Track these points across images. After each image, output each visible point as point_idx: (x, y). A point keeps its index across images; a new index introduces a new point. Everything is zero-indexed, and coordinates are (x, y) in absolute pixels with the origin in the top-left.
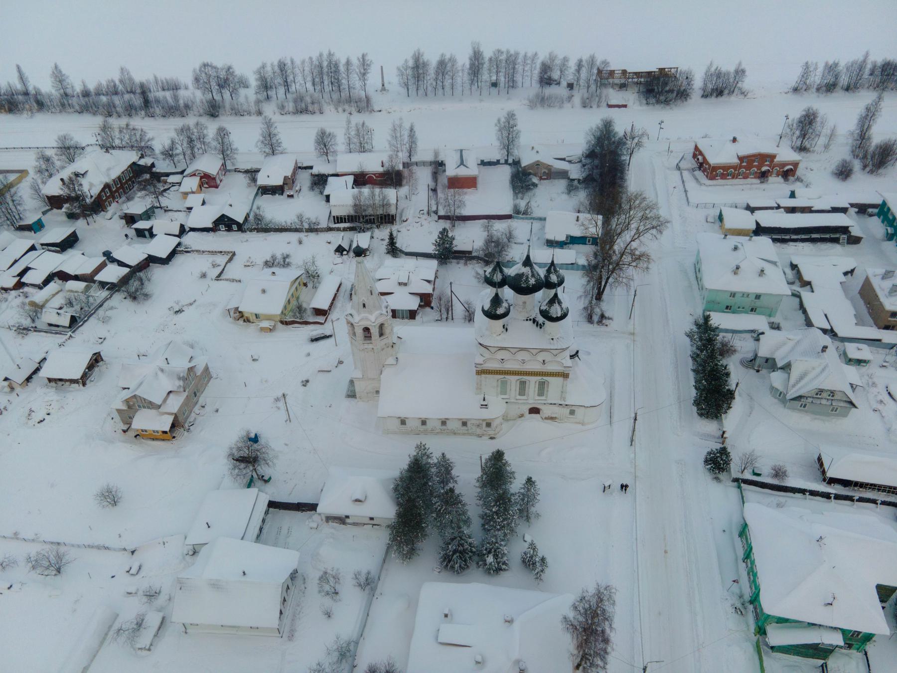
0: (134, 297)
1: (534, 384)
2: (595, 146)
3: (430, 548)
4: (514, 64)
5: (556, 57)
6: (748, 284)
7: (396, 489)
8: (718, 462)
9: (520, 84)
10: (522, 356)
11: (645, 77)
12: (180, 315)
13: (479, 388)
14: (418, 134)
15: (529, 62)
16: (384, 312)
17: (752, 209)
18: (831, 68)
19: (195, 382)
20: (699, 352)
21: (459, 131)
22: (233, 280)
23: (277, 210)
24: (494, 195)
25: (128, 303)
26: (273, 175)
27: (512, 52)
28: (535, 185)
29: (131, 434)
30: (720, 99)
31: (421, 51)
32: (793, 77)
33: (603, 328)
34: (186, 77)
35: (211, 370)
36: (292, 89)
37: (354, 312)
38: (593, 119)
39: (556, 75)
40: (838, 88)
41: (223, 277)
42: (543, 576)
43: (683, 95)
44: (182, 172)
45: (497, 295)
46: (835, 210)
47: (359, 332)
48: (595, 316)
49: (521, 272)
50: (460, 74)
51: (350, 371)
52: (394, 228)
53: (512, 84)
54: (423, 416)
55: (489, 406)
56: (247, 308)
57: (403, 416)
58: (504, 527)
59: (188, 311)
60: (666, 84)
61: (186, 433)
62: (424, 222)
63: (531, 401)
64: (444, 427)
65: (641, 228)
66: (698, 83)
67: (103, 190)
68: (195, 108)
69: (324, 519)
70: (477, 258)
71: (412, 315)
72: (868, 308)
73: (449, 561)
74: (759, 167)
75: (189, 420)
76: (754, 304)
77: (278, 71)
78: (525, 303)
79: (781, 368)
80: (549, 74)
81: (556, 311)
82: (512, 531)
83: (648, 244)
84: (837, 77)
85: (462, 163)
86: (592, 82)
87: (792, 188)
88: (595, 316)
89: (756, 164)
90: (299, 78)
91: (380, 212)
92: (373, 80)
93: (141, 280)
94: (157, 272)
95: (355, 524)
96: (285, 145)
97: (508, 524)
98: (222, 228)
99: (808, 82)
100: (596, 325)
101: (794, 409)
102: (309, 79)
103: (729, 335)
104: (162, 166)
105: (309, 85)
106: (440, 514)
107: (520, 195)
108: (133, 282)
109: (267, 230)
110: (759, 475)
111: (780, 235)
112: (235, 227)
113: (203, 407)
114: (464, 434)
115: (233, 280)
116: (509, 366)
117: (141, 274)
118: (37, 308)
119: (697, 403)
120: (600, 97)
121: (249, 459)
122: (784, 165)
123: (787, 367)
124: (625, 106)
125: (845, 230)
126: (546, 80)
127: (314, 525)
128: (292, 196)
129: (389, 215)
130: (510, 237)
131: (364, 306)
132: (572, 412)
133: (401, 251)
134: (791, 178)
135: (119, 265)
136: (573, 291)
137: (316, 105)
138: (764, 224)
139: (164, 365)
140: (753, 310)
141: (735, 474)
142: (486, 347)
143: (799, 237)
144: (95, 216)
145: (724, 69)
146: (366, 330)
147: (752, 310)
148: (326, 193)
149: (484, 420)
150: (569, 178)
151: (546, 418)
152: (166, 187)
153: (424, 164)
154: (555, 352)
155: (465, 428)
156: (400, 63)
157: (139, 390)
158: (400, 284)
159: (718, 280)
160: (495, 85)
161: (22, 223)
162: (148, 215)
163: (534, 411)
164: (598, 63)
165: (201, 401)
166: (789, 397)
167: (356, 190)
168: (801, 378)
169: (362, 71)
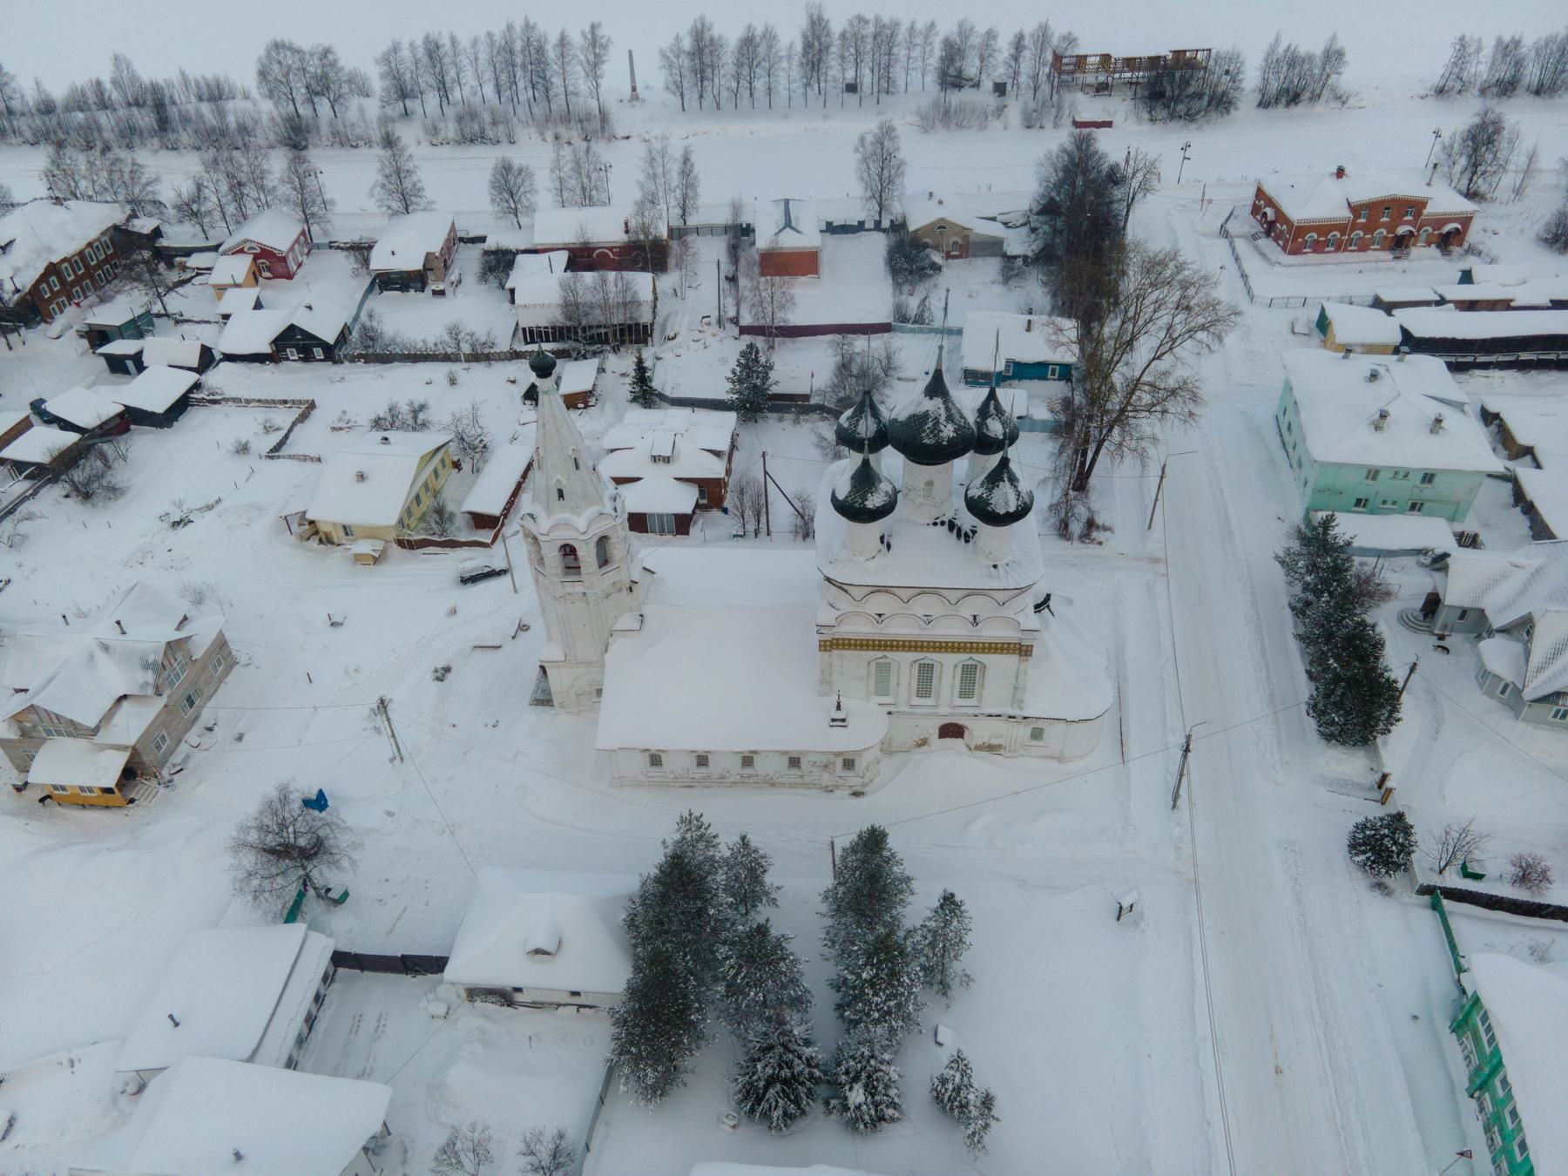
0: (85, 494)
1: (951, 671)
2: (1058, 186)
3: (713, 1069)
4: (891, 43)
5: (972, 29)
6: (1407, 449)
7: (631, 923)
8: (1382, 847)
9: (901, 82)
10: (923, 606)
11: (1146, 69)
12: (181, 531)
13: (826, 682)
14: (700, 169)
15: (919, 40)
16: (608, 509)
17: (1389, 308)
18: (1508, 50)
19: (188, 676)
20: (1311, 597)
21: (787, 169)
22: (305, 458)
23: (407, 319)
24: (855, 287)
25: (73, 504)
26: (403, 248)
27: (886, 19)
28: (937, 268)
29: (33, 795)
30: (1295, 110)
31: (708, 19)
32: (1435, 68)
33: (1091, 549)
34: (243, 76)
35: (232, 646)
36: (456, 95)
37: (537, 509)
38: (1056, 140)
39: (971, 68)
40: (1519, 91)
41: (285, 451)
42: (987, 1138)
43: (1221, 102)
44: (216, 248)
45: (866, 463)
47: (552, 555)
48: (1076, 525)
49: (922, 409)
50: (785, 64)
51: (541, 647)
52: (648, 354)
53: (886, 86)
54: (701, 747)
55: (850, 721)
56: (326, 513)
57: (654, 746)
58: (889, 1013)
59: (201, 523)
60: (1185, 82)
61: (162, 790)
62: (713, 342)
63: (944, 710)
64: (748, 771)
65: (1179, 329)
66: (1251, 78)
67: (44, 278)
68: (259, 132)
69: (464, 994)
70: (820, 408)
71: (682, 524)
73: (759, 1101)
74: (1391, 227)
75: (173, 760)
76: (1420, 493)
77: (425, 60)
78: (930, 484)
79: (1502, 631)
80: (958, 64)
81: (1004, 499)
82: (907, 1018)
83: (1187, 362)
84: (1519, 64)
85: (788, 224)
86: (1043, 78)
87: (1465, 265)
88: (1076, 525)
89: (1385, 219)
90: (469, 77)
91: (618, 318)
92: (614, 79)
93: (103, 457)
94: (142, 443)
95: (536, 1005)
96: (429, 193)
97: (899, 1006)
98: (292, 353)
99: (1465, 75)
100: (1076, 543)
101: (1537, 722)
102: (488, 75)
103: (1372, 560)
104: (178, 235)
105: (489, 90)
106: (733, 990)
107: (906, 288)
108: (84, 464)
109: (386, 359)
110: (1478, 877)
111: (1463, 355)
112: (318, 352)
113: (210, 729)
114: (793, 786)
115: (305, 458)
116: (898, 629)
117: (106, 448)
119: (1317, 710)
120: (1060, 108)
121: (295, 854)
122: (1440, 221)
123: (1523, 628)
126: (952, 79)
127: (441, 1009)
128: (441, 293)
129: (637, 325)
130: (888, 367)
131: (561, 494)
132: (1037, 734)
133: (662, 397)
134: (1456, 250)
135: (62, 428)
136: (1034, 461)
137: (501, 127)
138: (1419, 331)
139: (109, 633)
141: (1427, 877)
142: (841, 587)
143: (1493, 358)
144: (23, 331)
146: (569, 551)
147: (1413, 507)
148: (508, 285)
149: (838, 754)
150: (1004, 256)
151: (978, 748)
152: (185, 276)
153: (712, 230)
154: (1000, 596)
155: (795, 771)
156: (667, 42)
157: (43, 694)
158: (655, 459)
159: (1338, 440)
160: (852, 88)
162: (138, 327)
163: (952, 731)
164: (1055, 41)
165: (206, 717)
166: (1529, 694)
167: (569, 274)
168: (1557, 653)
169: (591, 57)
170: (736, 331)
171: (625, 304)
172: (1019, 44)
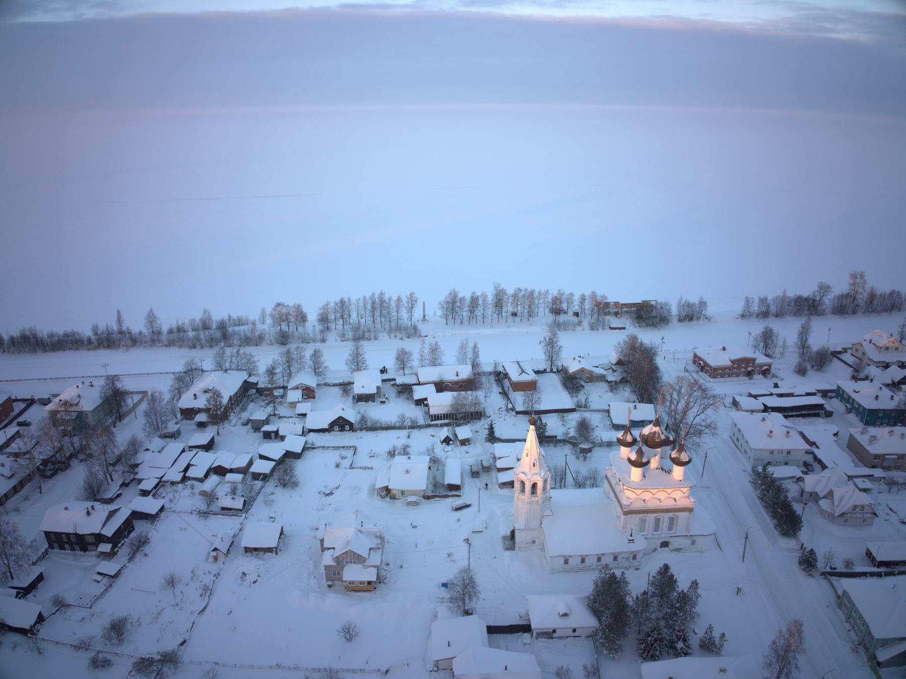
3: (630, 641)
8: (808, 562)
17: (755, 397)
18: (763, 301)
21: (515, 349)
22: (366, 468)
32: (739, 307)
39: (564, 306)
46: (808, 394)
53: (531, 314)
63: (663, 536)
66: (674, 310)
72: (857, 457)
74: (746, 368)
79: (824, 497)
84: (768, 306)
85: (523, 371)
92: (418, 314)
98: (336, 428)
112: (347, 427)
115: (366, 468)
118: (210, 497)
122: (761, 366)
123: (830, 495)
124: (624, 328)
125: (821, 407)
132: (693, 543)
134: (769, 376)
138: (769, 405)
140: (786, 464)
145: (692, 301)
151: (674, 550)
160: (514, 314)
161: (165, 431)
163: (665, 544)
166: (836, 514)
168: (841, 500)
170: (514, 413)
171: (476, 404)
172: (583, 299)
